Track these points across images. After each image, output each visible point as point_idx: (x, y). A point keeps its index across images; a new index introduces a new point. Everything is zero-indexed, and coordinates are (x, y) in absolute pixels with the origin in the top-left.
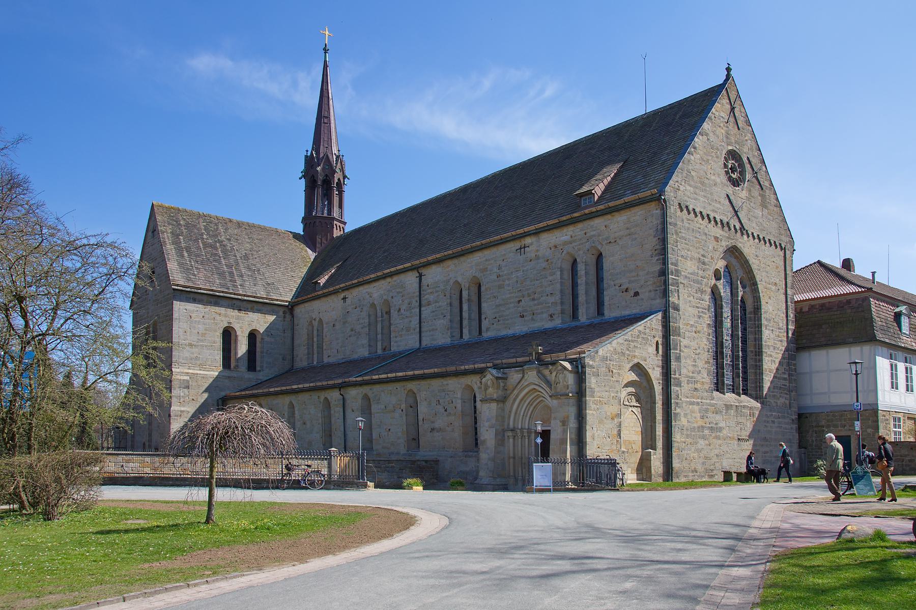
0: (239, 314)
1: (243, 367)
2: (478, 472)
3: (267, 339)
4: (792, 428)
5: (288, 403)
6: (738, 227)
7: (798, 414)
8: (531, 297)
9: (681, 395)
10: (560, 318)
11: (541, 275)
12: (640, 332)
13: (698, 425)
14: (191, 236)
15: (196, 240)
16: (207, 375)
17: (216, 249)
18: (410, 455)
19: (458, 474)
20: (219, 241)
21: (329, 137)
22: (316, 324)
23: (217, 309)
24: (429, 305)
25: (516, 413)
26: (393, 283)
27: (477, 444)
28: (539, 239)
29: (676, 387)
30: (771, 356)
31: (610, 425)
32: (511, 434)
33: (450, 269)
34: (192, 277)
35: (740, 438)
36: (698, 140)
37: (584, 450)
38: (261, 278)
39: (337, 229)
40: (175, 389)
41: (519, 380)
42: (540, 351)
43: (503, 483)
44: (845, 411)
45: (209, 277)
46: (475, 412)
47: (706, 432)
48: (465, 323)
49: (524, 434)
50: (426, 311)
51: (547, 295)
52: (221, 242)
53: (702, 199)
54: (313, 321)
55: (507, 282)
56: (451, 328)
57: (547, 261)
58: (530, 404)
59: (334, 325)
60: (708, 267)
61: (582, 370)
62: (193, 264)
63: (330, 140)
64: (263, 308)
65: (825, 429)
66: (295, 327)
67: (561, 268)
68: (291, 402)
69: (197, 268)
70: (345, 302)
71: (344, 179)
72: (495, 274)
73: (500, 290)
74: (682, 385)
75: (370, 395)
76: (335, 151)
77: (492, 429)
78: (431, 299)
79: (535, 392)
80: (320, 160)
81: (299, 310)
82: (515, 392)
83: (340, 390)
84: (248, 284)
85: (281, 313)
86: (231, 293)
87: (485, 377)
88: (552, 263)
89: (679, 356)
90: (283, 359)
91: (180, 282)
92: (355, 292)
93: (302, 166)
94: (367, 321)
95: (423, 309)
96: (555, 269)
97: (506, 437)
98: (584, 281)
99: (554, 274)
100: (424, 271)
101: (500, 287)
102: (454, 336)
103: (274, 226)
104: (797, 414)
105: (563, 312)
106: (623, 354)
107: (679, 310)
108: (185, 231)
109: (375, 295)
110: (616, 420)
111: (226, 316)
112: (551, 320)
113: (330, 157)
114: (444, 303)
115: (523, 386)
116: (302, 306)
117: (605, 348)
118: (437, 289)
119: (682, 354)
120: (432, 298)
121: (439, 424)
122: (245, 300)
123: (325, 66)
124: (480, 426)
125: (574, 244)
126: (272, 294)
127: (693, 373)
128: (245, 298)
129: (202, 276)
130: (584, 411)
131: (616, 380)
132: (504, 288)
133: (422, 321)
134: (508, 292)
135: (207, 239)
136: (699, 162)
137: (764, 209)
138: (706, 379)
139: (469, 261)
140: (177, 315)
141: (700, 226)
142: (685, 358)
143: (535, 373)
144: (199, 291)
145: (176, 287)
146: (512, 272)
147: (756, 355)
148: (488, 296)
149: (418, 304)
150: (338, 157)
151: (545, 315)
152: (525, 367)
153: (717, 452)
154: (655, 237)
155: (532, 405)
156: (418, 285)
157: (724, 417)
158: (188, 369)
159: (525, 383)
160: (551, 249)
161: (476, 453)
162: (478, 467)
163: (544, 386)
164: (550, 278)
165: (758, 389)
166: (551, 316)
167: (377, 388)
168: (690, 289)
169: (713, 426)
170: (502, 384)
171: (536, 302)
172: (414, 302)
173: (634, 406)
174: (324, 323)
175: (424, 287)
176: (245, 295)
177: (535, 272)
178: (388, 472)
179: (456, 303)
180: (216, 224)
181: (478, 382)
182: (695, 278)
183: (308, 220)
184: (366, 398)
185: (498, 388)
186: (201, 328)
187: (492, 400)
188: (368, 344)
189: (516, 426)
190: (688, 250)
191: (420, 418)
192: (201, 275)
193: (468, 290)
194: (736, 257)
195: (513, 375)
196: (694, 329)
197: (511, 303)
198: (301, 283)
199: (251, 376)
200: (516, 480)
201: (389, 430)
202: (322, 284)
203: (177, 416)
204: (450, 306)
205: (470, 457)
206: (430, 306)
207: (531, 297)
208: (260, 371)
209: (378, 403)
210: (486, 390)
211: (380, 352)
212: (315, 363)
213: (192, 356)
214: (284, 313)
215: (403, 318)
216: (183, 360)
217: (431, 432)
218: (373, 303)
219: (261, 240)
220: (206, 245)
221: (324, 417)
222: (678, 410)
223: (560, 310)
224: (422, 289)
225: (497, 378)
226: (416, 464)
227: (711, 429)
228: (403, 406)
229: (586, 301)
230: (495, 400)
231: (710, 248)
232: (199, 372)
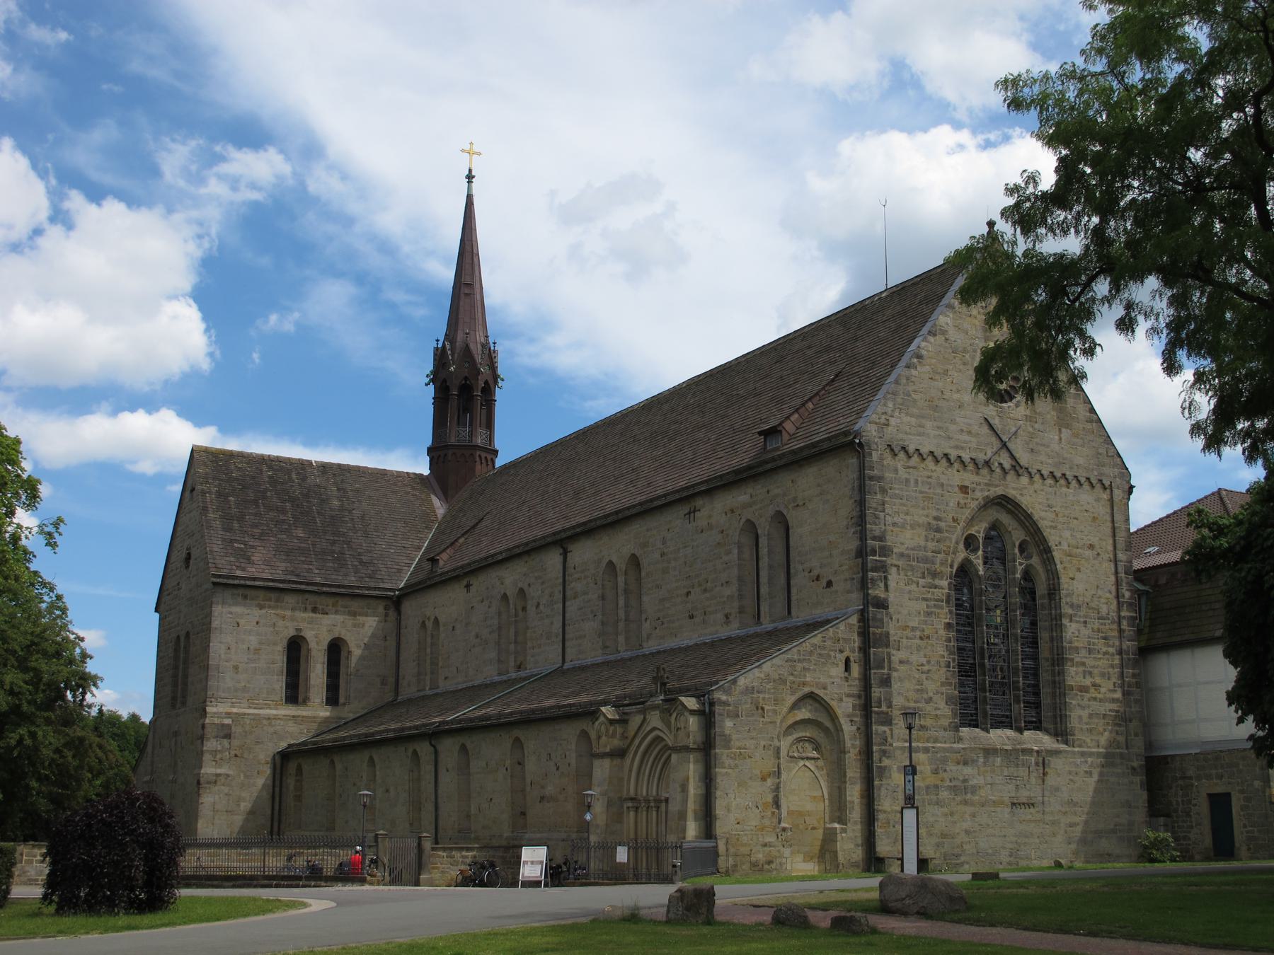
6: (1007, 466)
8: (703, 588)
11: (714, 554)
12: (814, 646)
13: (927, 784)
16: (259, 715)
24: (575, 598)
29: (882, 725)
30: (1083, 664)
31: (762, 791)
35: (1016, 801)
36: (924, 344)
47: (944, 794)
50: (572, 607)
53: (933, 433)
59: (453, 627)
60: (946, 534)
65: (1193, 781)
66: (402, 631)
70: (468, 591)
74: (894, 722)
81: (408, 607)
82: (637, 742)
86: (301, 583)
87: (597, 719)
89: (886, 679)
95: (568, 604)
98: (766, 564)
102: (607, 647)
104: (1144, 759)
105: (741, 611)
106: (784, 682)
110: (769, 782)
111: (293, 619)
113: (472, 346)
117: (750, 675)
119: (894, 674)
121: (550, 790)
127: (916, 702)
130: (712, 770)
133: (566, 622)
137: (1063, 430)
138: (941, 710)
146: (679, 549)
147: (1053, 665)
151: (720, 616)
153: (965, 825)
154: (851, 498)
164: (726, 558)
165: (1059, 720)
168: (909, 573)
171: (708, 595)
173: (808, 758)
175: (570, 570)
176: (323, 585)
182: (921, 553)
190: (907, 514)
191: (528, 781)
194: (1009, 512)
196: (918, 633)
201: (491, 799)
208: (344, 704)
214: (386, 608)
216: (223, 692)
222: (886, 762)
227: (954, 790)
228: (508, 762)
231: (952, 504)
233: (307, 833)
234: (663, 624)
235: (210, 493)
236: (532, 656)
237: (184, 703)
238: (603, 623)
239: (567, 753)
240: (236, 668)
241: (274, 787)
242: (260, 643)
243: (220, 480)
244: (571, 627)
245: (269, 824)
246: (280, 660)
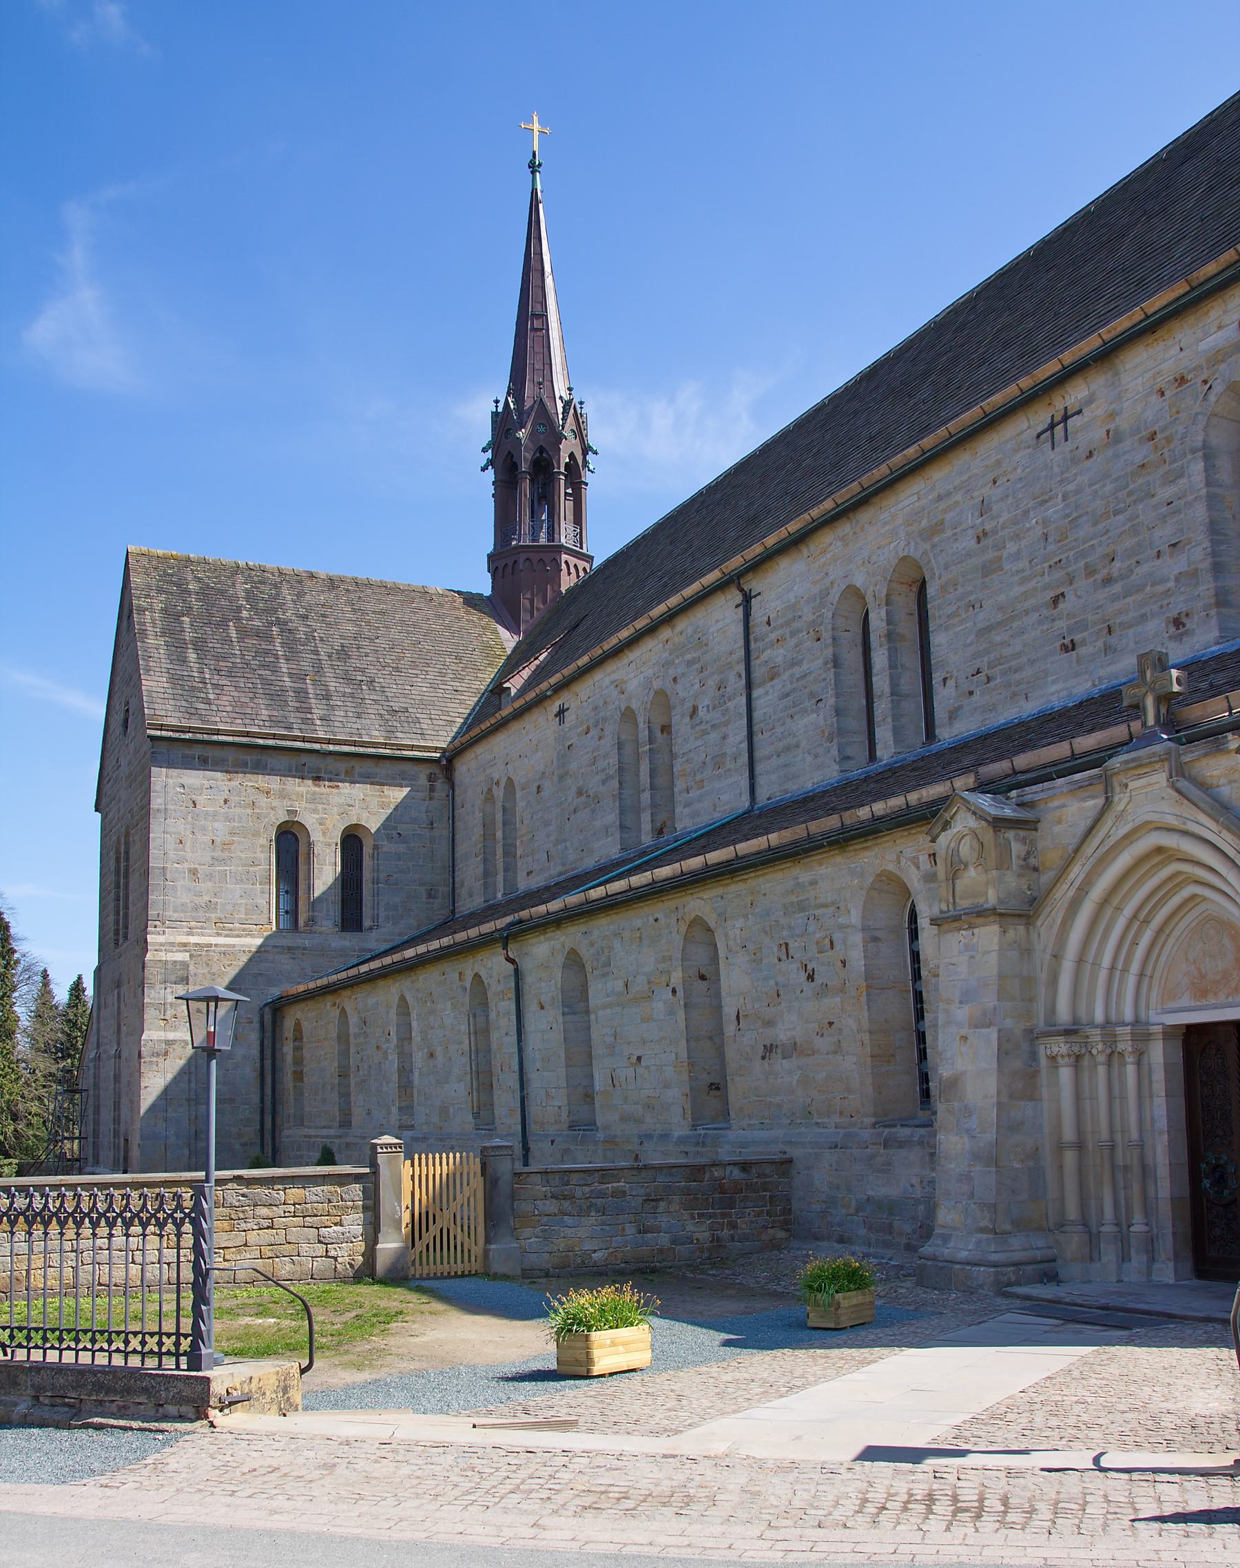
0: (317, 789)
1: (328, 924)
2: (931, 1210)
3: (387, 847)
5: (397, 1000)
8: (1098, 577)
10: (1214, 622)
11: (1129, 494)
14: (211, 615)
15: (223, 623)
16: (234, 946)
17: (270, 639)
18: (701, 1142)
19: (858, 1209)
20: (279, 622)
21: (547, 361)
22: (499, 793)
23: (261, 781)
24: (772, 679)
25: (1080, 961)
26: (676, 639)
27: (926, 1094)
28: (1117, 374)
32: (1064, 1049)
33: (829, 556)
34: (202, 706)
38: (375, 698)
39: (569, 574)
40: (152, 986)
41: (1089, 822)
42: (1176, 688)
43: (1039, 1254)
45: (244, 705)
46: (917, 976)
48: (882, 707)
49: (1121, 1047)
50: (765, 698)
51: (1159, 555)
52: (281, 623)
54: (495, 787)
55: (1011, 548)
56: (841, 732)
57: (1152, 436)
58: (1142, 916)
59: (539, 787)
62: (207, 676)
63: (547, 367)
64: (377, 770)
67: (1205, 446)
68: (403, 999)
69: (216, 686)
70: (561, 722)
71: (585, 453)
72: (970, 532)
73: (987, 579)
75: (586, 953)
76: (560, 389)
77: (985, 1031)
78: (779, 659)
79: (1163, 863)
80: (525, 416)
81: (465, 768)
82: (1077, 872)
83: (505, 947)
84: (342, 713)
85: (423, 781)
86: (295, 739)
87: (946, 825)
90: (430, 896)
92: (585, 690)
93: (485, 434)
94: (613, 760)
96: (1185, 455)
97: (1043, 1061)
99: (1181, 476)
100: (754, 584)
101: (987, 570)
103: (417, 582)
108: (196, 604)
109: (633, 685)
111: (283, 795)
112: (1179, 638)
113: (548, 404)
114: (815, 661)
115: (1112, 841)
116: (470, 755)
118: (796, 625)
120: (777, 655)
121: (788, 1029)
122: (331, 753)
123: (534, 203)
124: (935, 1026)
126: (399, 735)
128: (331, 747)
129: (227, 703)
133: (756, 728)
134: (1016, 578)
135: (250, 619)
139: (885, 515)
140: (160, 801)
143: (1160, 778)
144: (215, 738)
145: (158, 733)
148: (950, 610)
149: (743, 682)
150: (567, 404)
152: (1116, 762)
155: (1146, 922)
156: (740, 629)
158: (189, 934)
159: (1113, 829)
160: (1163, 394)
161: (922, 1131)
162: (932, 1182)
163: (1207, 827)
166: (1177, 623)
167: (602, 926)
170: (1017, 848)
171: (1117, 588)
172: (732, 678)
176: (329, 742)
177: (1108, 488)
178: (603, 1211)
179: (853, 657)
180: (275, 586)
181: (923, 859)
183: (500, 563)
184: (574, 961)
185: (1003, 862)
186: (220, 829)
187: (981, 913)
188: (618, 823)
189: (1083, 1015)
191: (729, 1011)
192: (225, 700)
193: (887, 604)
195: (1064, 806)
197: (1027, 613)
198: (476, 704)
199: (347, 944)
200: (1093, 1239)
201: (639, 1059)
202: (513, 692)
203: (158, 1055)
204: (835, 666)
205: (901, 1144)
206: (776, 681)
207: (1098, 577)
209: (603, 975)
210: (953, 876)
211: (647, 839)
212: (499, 896)
213: (198, 900)
214: (431, 778)
215: (705, 732)
216: (175, 911)
217: (763, 1058)
218: (628, 708)
219: (383, 613)
220: (243, 633)
221: (476, 1033)
223: (1212, 592)
224: (751, 637)
225: (998, 824)
226: (707, 1176)
228: (677, 977)
230: (993, 911)
232: (213, 940)
233: (312, 1132)
234: (989, 680)
235: (152, 610)
236: (687, 805)
237: (126, 938)
238: (838, 712)
239: (837, 937)
240: (194, 872)
241: (262, 1059)
242: (232, 834)
243: (167, 593)
244: (766, 735)
245: (258, 1117)
246: (267, 861)
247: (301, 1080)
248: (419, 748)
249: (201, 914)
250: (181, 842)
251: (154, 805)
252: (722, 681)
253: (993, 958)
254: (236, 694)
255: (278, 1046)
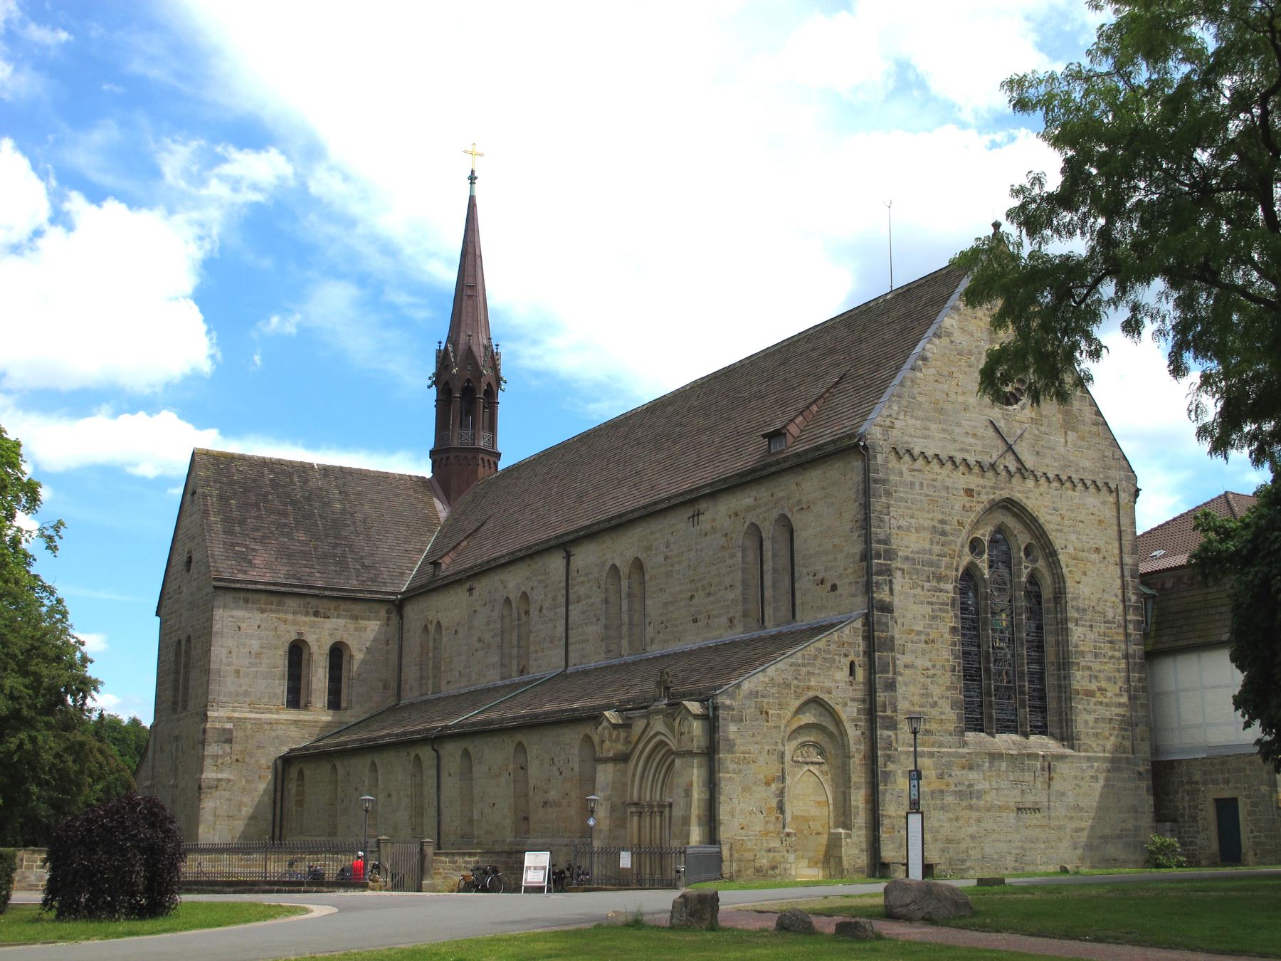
4: (1138, 788)
6: (1012, 468)
7: (1152, 762)
9: (897, 742)
11: (718, 558)
12: (818, 650)
13: (932, 789)
16: (261, 719)
31: (767, 796)
35: (1021, 806)
36: (929, 346)
37: (717, 832)
44: (1227, 756)
47: (950, 799)
50: (575, 610)
59: (456, 631)
60: (951, 538)
61: (714, 714)
66: (404, 635)
70: (471, 595)
74: (899, 726)
81: (411, 611)
82: (640, 746)
86: (303, 587)
87: (600, 724)
88: (731, 538)
89: (891, 683)
91: (226, 574)
94: (498, 625)
95: (571, 607)
98: (771, 568)
104: (1150, 764)
106: (788, 686)
107: (893, 610)
110: (773, 786)
111: (294, 623)
113: (474, 348)
117: (754, 679)
119: (899, 678)
121: (553, 795)
125: (759, 511)
130: (716, 775)
131: (774, 725)
132: (672, 576)
133: (570, 626)
136: (933, 378)
137: (1069, 433)
141: (935, 477)
142: (906, 684)
147: (1059, 669)
151: (724, 620)
153: (970, 830)
154: (855, 501)
157: (987, 773)
164: (730, 562)
165: (1064, 724)
168: (914, 577)
169: (963, 788)
171: (712, 599)
173: (812, 763)
174: (443, 628)
175: (573, 574)
176: (325, 589)
182: (926, 557)
186: (255, 644)
190: (912, 517)
191: (531, 786)
194: (1015, 515)
196: (923, 637)
208: (346, 709)
216: (224, 696)
222: (891, 767)
227: (959, 794)
228: (511, 767)
229: (774, 597)
231: (956, 508)
236: (535, 660)
237: (185, 708)
238: (606, 627)
239: (570, 758)
240: (237, 672)
242: (262, 647)
243: (221, 483)
244: (574, 631)
247: (302, 806)
248: (381, 593)
249: (240, 698)
250: (230, 652)
251: (215, 629)
252: (555, 596)
253: (611, 775)
254: (266, 555)
255: (286, 783)
